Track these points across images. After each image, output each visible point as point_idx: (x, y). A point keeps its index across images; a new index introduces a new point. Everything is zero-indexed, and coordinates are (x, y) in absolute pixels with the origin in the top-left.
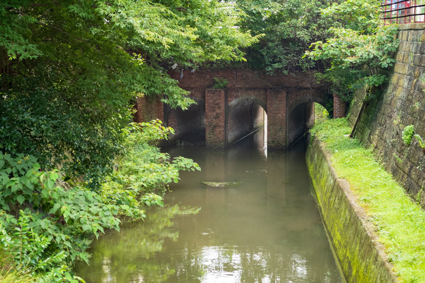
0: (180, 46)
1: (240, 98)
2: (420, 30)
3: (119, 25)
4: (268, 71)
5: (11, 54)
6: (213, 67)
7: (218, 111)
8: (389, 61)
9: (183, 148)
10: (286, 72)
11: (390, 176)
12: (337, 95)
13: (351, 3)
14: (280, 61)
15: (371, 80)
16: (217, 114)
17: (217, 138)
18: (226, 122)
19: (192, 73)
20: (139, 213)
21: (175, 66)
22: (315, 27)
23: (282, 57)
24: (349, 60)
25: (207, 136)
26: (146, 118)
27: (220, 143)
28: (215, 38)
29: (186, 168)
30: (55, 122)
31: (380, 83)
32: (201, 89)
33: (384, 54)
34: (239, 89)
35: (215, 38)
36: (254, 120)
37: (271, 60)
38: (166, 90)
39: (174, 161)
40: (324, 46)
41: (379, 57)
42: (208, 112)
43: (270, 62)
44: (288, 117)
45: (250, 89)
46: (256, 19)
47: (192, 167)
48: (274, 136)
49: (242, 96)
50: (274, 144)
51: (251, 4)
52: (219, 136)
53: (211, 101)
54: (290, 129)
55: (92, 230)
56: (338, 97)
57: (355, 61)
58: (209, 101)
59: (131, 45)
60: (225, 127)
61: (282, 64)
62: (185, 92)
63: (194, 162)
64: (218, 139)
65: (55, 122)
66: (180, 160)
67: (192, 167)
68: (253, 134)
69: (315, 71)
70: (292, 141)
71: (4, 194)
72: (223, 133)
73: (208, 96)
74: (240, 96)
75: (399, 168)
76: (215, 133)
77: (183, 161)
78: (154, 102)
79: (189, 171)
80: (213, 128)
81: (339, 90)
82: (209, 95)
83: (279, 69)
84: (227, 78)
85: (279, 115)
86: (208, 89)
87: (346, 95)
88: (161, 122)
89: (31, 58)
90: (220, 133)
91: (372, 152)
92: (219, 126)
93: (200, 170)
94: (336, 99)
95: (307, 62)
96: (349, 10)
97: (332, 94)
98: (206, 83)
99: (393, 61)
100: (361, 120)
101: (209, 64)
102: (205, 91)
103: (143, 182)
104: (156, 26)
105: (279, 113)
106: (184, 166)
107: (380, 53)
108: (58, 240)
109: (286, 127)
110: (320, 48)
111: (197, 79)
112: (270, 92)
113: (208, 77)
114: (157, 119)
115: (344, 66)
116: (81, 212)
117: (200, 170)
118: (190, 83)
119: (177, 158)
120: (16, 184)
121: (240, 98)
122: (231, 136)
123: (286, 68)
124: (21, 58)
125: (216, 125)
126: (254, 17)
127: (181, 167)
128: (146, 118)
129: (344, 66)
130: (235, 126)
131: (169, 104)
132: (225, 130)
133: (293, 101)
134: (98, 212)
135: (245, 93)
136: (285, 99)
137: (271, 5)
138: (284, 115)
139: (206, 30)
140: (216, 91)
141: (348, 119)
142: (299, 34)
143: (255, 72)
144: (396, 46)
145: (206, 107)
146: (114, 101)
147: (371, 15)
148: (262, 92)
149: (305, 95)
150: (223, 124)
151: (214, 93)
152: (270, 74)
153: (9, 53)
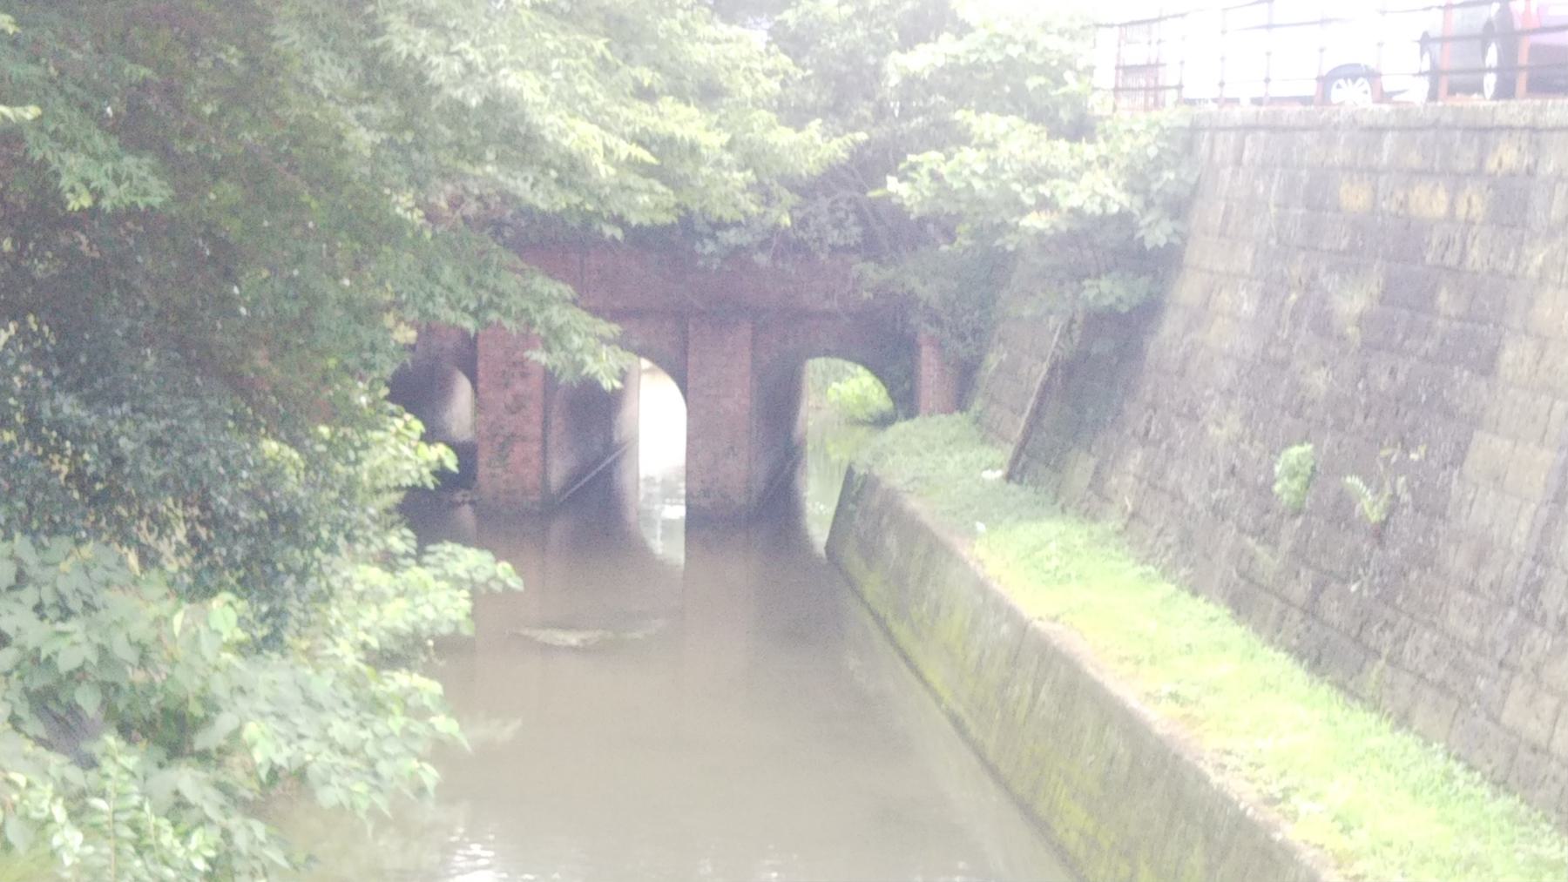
2: (1305, 129)
5: (73, 190)
11: (1223, 612)
16: (516, 397)
18: (546, 424)
22: (868, 114)
30: (157, 426)
31: (1135, 301)
39: (427, 559)
47: (494, 577)
60: (544, 441)
63: (497, 561)
65: (157, 426)
66: (449, 554)
67: (494, 577)
68: (610, 467)
69: (855, 257)
71: (27, 680)
72: (536, 461)
75: (1260, 586)
77: (461, 557)
79: (484, 591)
80: (502, 446)
87: (962, 338)
89: (142, 206)
91: (1118, 533)
92: (524, 439)
96: (996, 58)
100: (1045, 422)
103: (367, 631)
107: (1138, 201)
108: (241, 840)
115: (1012, 242)
116: (307, 745)
120: (74, 644)
122: (558, 472)
124: (106, 204)
125: (513, 435)
132: (544, 451)
138: (745, 401)
141: (977, 420)
144: (1192, 180)
150: (538, 431)
153: (67, 188)
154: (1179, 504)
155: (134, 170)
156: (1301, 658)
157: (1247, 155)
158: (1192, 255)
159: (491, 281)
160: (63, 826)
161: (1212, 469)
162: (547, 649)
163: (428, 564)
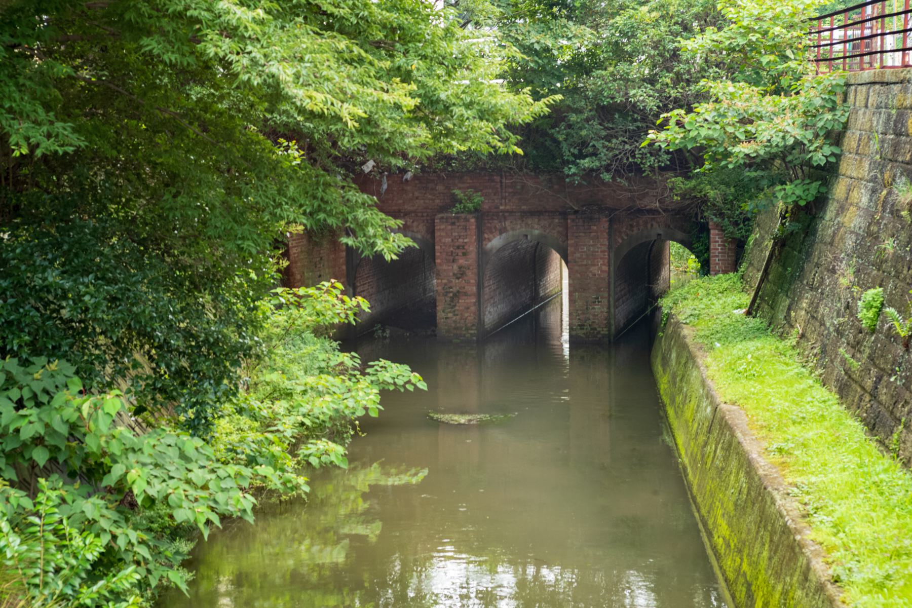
0: (380, 123)
1: (511, 233)
2: (895, 83)
3: (249, 79)
4: (568, 176)
5: (17, 144)
6: (452, 167)
7: (462, 261)
8: (827, 150)
9: (388, 341)
10: (607, 177)
12: (717, 226)
13: (745, 28)
14: (595, 154)
15: (790, 193)
16: (460, 268)
17: (461, 319)
18: (480, 286)
19: (406, 180)
20: (294, 483)
21: (369, 166)
22: (668, 81)
23: (599, 145)
24: (742, 150)
25: (440, 315)
26: (308, 278)
27: (467, 329)
28: (454, 104)
29: (395, 384)
30: (113, 289)
31: (810, 199)
32: (425, 214)
33: (817, 136)
34: (507, 214)
35: (454, 104)
36: (540, 280)
37: (576, 152)
38: (350, 219)
39: (368, 370)
40: (688, 119)
41: (806, 142)
42: (440, 264)
43: (573, 155)
44: (612, 274)
45: (532, 213)
46: (540, 61)
48: (583, 313)
49: (513, 229)
50: (585, 331)
51: (529, 32)
52: (466, 315)
53: (448, 240)
54: (618, 300)
55: (195, 521)
56: (719, 230)
57: (756, 151)
58: (443, 240)
59: (274, 121)
60: (479, 295)
61: (600, 160)
62: (392, 222)
63: (412, 372)
64: (462, 321)
65: (113, 289)
66: (382, 367)
67: (409, 382)
68: (537, 312)
69: (670, 174)
70: (622, 324)
72: (473, 308)
73: (439, 226)
74: (509, 228)
75: (853, 380)
76: (457, 308)
77: (389, 369)
78: (326, 244)
79: (402, 390)
80: (452, 299)
81: (722, 215)
82: (442, 227)
83: (592, 170)
84: (481, 191)
85: (594, 269)
86: (440, 215)
87: (736, 224)
88: (340, 286)
89: (61, 153)
90: (468, 308)
92: (466, 294)
93: (426, 389)
94: (714, 234)
95: (652, 155)
96: (742, 41)
97: (708, 223)
98: (437, 201)
99: (836, 150)
101: (442, 160)
102: (433, 220)
103: (304, 416)
104: (328, 80)
105: (594, 265)
106: (392, 381)
107: (809, 134)
108: (121, 543)
109: (609, 295)
110: (679, 124)
111: (417, 194)
112: (573, 221)
113: (440, 188)
114: (333, 281)
115: (731, 162)
116: (171, 483)
117: (426, 389)
118: (401, 201)
119: (376, 363)
120: (31, 423)
121: (511, 233)
122: (491, 314)
123: (607, 169)
124: (39, 153)
125: (458, 292)
126: (536, 58)
127: (384, 382)
128: (308, 278)
129: (731, 162)
130: (500, 294)
131: (358, 248)
133: (623, 239)
134: (208, 481)
135: (520, 222)
136: (606, 235)
137: (572, 32)
138: (605, 268)
139: (436, 89)
140: (458, 218)
141: (742, 277)
142: (634, 95)
143: (542, 178)
144: (843, 120)
145: (438, 254)
146: (239, 242)
147: (789, 53)
148: (557, 221)
149: (649, 226)
150: (474, 289)
151: (453, 224)
152: (574, 180)
153: (13, 143)
154: (823, 328)
155: (61, 130)
156: (866, 425)
157: (870, 100)
158: (844, 167)
159: (320, 195)
160: (7, 534)
161: (839, 305)
162: (447, 425)
163: (369, 374)
